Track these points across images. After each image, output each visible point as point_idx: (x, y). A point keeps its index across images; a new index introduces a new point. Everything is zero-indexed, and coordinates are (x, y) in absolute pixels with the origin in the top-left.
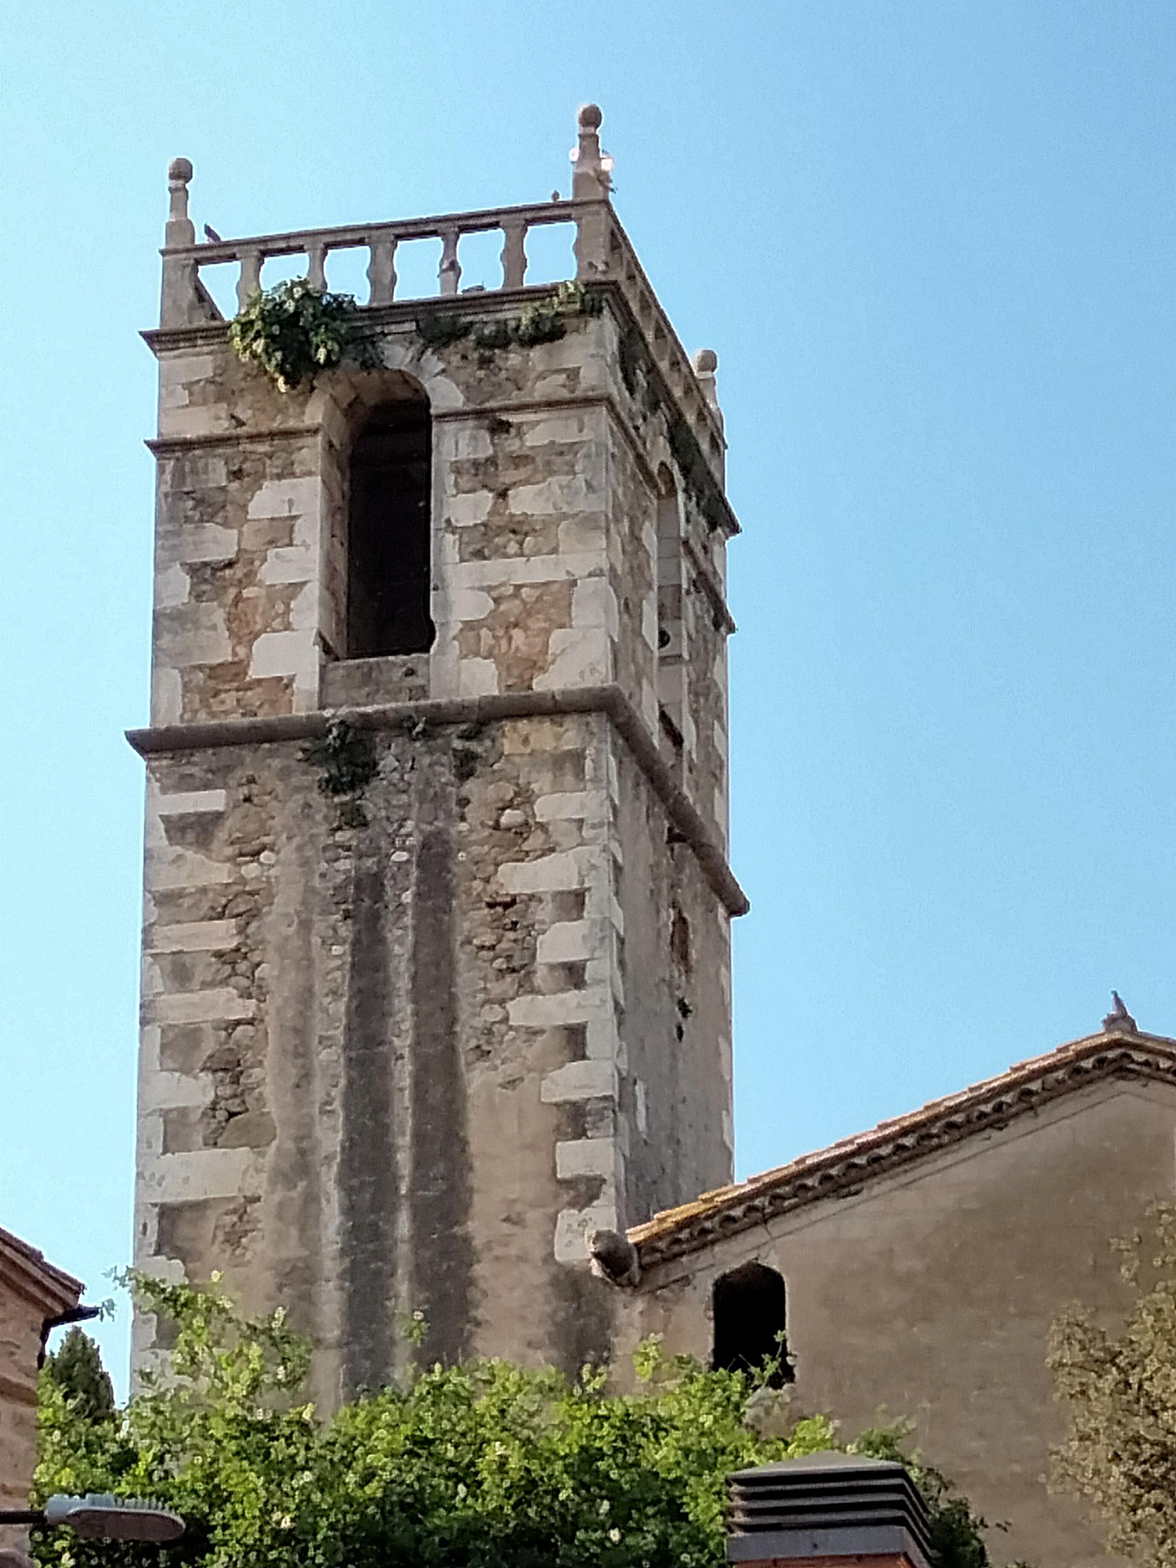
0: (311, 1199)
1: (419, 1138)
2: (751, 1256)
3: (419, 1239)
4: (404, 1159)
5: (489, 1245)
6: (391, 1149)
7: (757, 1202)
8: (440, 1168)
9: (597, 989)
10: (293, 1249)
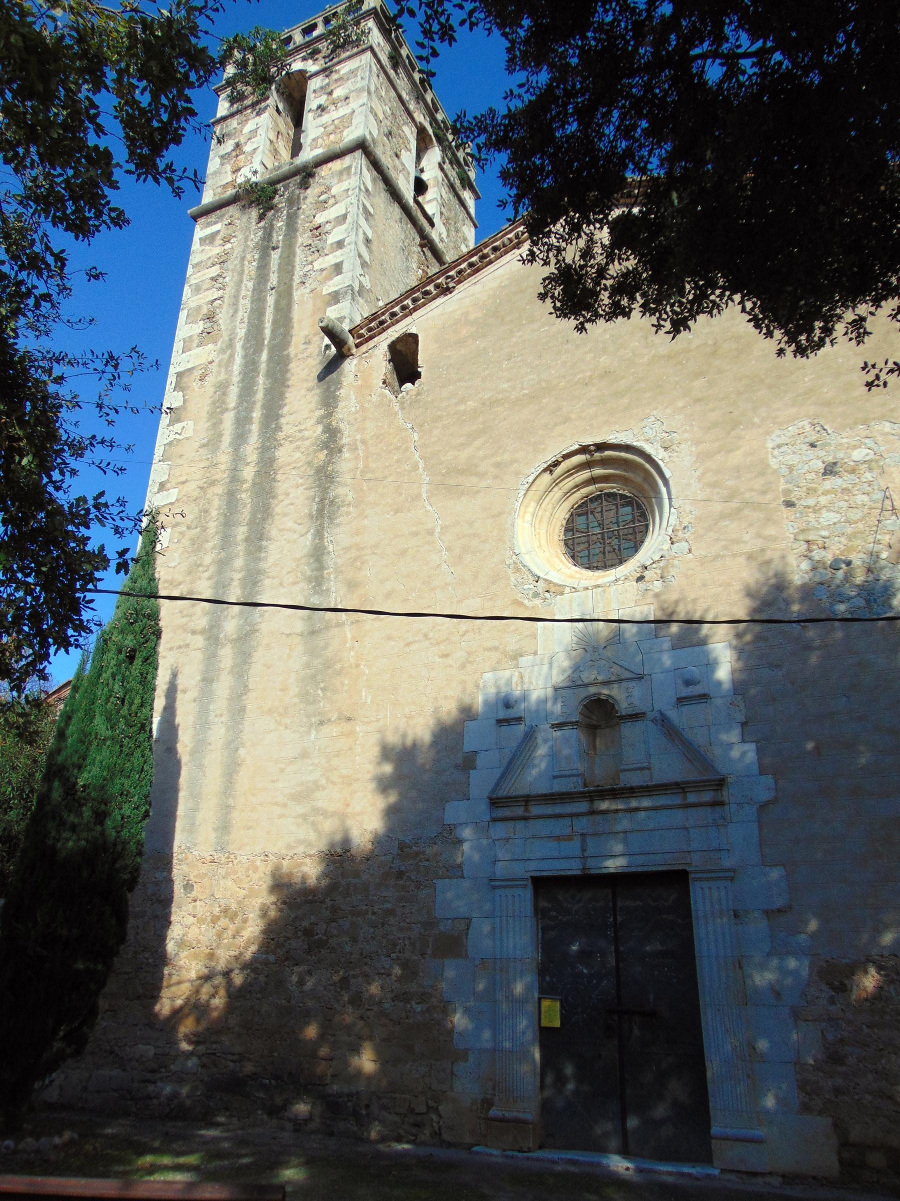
0: (232, 356)
1: (275, 322)
2: (404, 330)
3: (270, 359)
4: (268, 332)
5: (296, 355)
6: (263, 329)
7: (405, 303)
8: (282, 331)
9: (349, 247)
10: (222, 377)
